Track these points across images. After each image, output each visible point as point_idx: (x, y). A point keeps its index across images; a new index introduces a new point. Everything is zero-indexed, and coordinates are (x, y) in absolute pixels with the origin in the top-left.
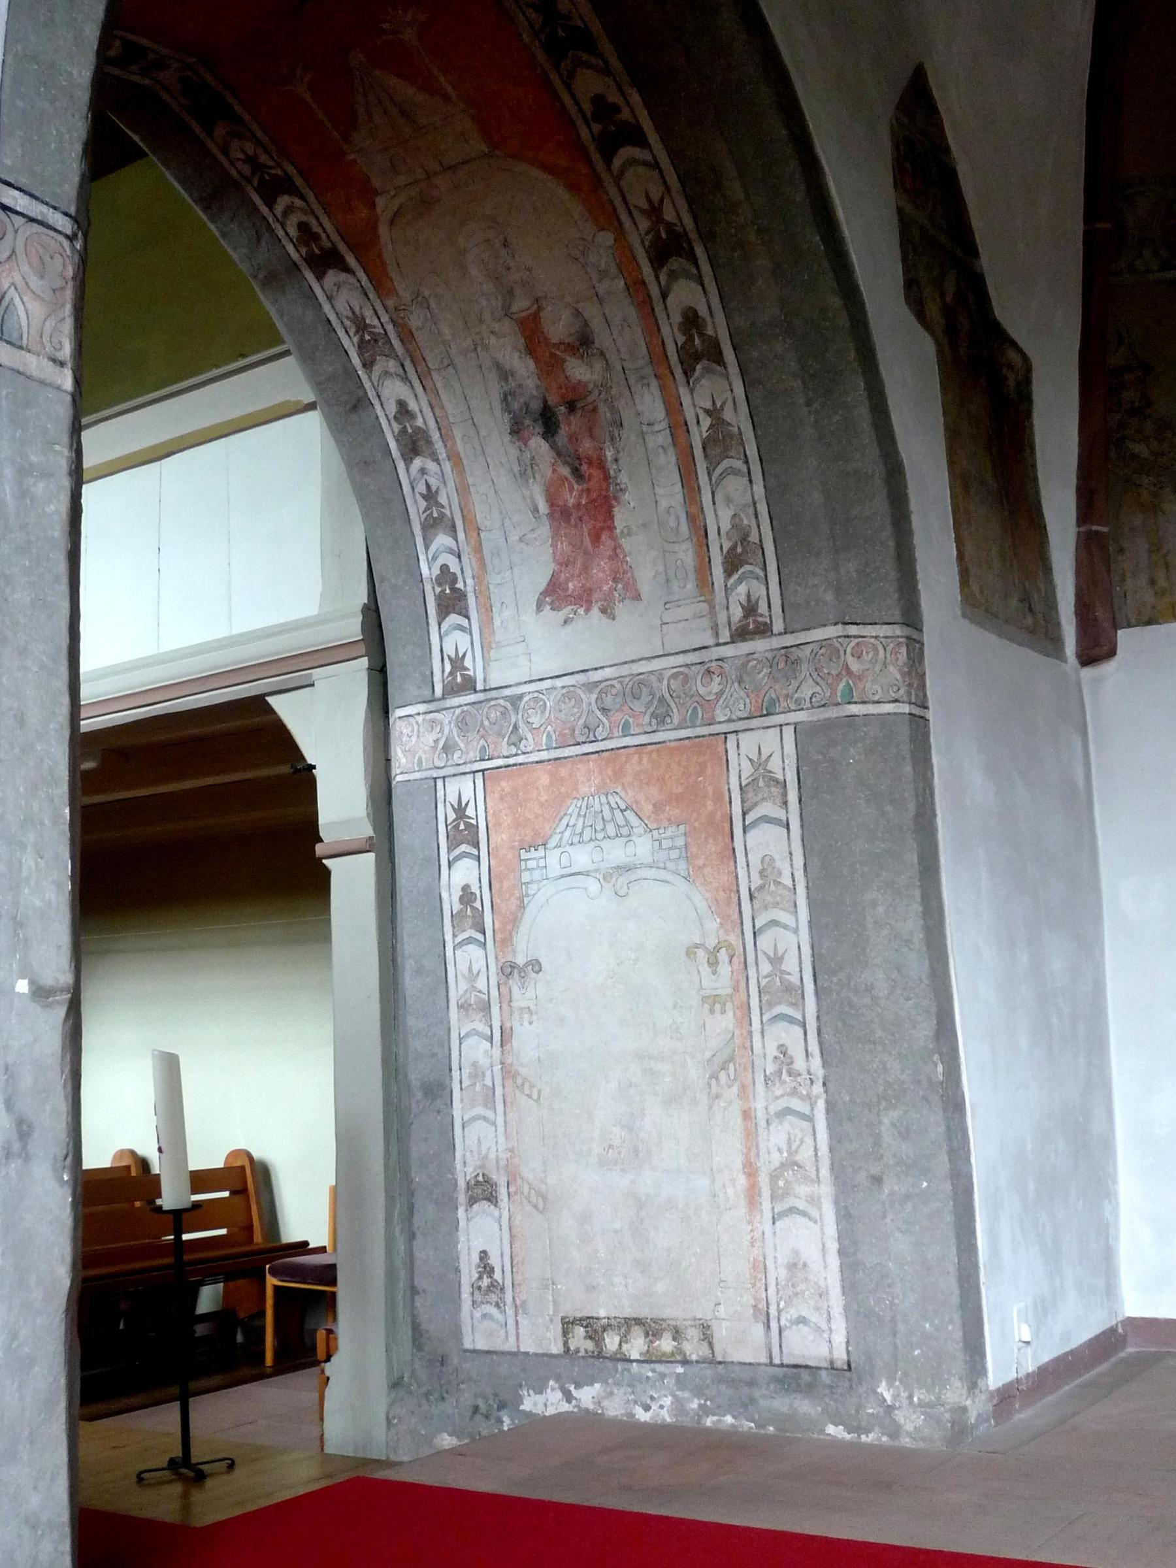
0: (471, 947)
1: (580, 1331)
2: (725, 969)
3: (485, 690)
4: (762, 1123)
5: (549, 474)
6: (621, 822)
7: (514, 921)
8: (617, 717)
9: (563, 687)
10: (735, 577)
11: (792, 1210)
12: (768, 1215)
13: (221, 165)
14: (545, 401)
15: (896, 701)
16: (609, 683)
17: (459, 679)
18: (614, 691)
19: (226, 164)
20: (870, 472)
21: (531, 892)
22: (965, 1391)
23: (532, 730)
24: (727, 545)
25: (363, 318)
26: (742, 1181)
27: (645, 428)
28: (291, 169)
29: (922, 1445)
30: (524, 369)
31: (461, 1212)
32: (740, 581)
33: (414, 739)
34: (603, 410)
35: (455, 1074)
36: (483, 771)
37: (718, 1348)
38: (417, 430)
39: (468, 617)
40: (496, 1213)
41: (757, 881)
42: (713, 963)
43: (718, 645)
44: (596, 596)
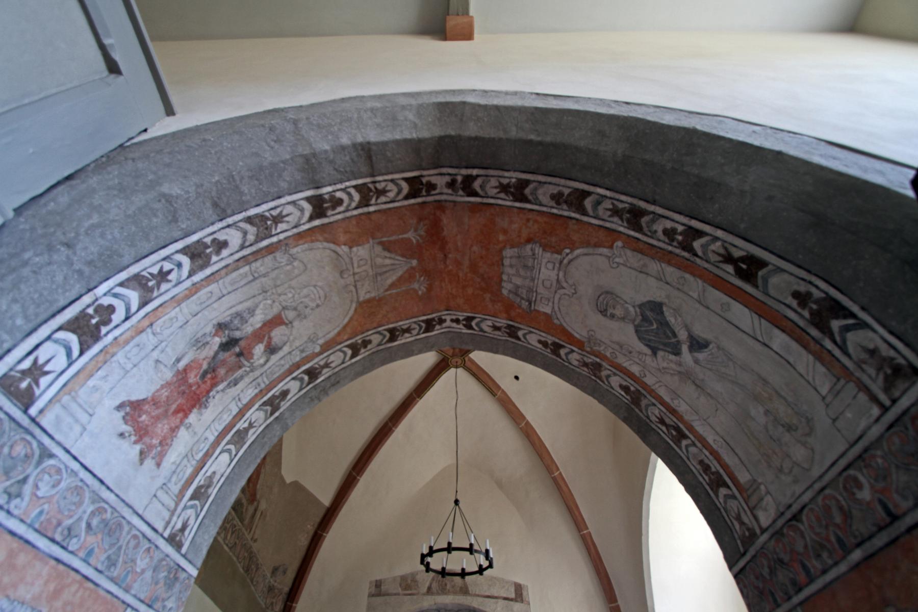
3: (33, 420)
9: (82, 480)
13: (386, 174)
14: (241, 339)
16: (106, 506)
17: (24, 385)
18: (104, 517)
19: (386, 177)
24: (202, 483)
25: (282, 222)
30: (257, 321)
38: (209, 257)
39: (82, 353)
43: (162, 535)
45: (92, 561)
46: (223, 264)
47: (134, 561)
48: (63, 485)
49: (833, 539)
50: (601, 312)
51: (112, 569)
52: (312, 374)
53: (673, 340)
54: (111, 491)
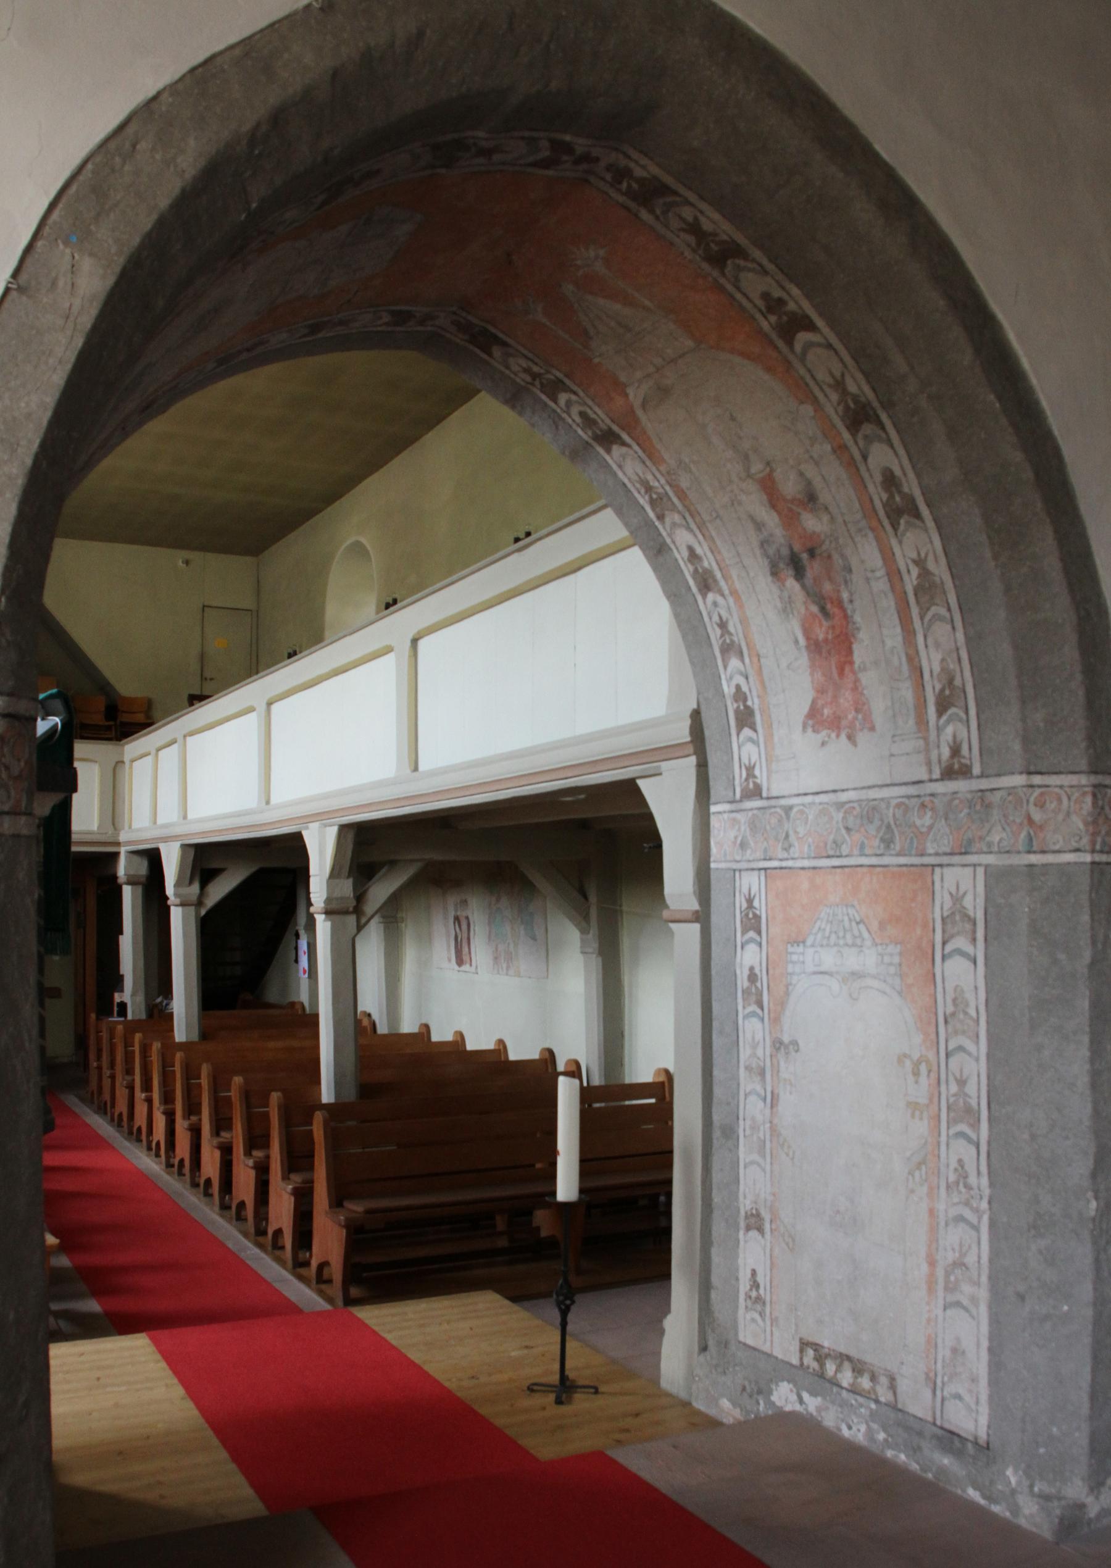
0: (754, 1020)
1: (810, 1353)
2: (923, 1080)
3: (768, 798)
4: (942, 1224)
5: (803, 610)
6: (856, 933)
7: (782, 1004)
8: (857, 837)
9: (820, 804)
10: (944, 718)
11: (958, 1304)
12: (941, 1302)
14: (791, 549)
15: (1077, 850)
16: (851, 805)
18: (855, 813)
20: (1060, 621)
21: (794, 982)
22: (1085, 1490)
23: (798, 838)
24: (938, 687)
25: (648, 482)
26: (925, 1268)
27: (869, 575)
28: (558, 374)
29: (1034, 1530)
30: (771, 520)
31: (741, 1233)
32: (948, 722)
33: (722, 833)
34: (835, 556)
35: (741, 1122)
36: (765, 869)
37: (900, 1399)
39: (755, 731)
40: (763, 1242)
41: (950, 1009)
42: (916, 1073)
43: (931, 780)
44: (844, 723)
46: (709, 554)
48: (811, 817)
51: (892, 846)
54: (847, 790)
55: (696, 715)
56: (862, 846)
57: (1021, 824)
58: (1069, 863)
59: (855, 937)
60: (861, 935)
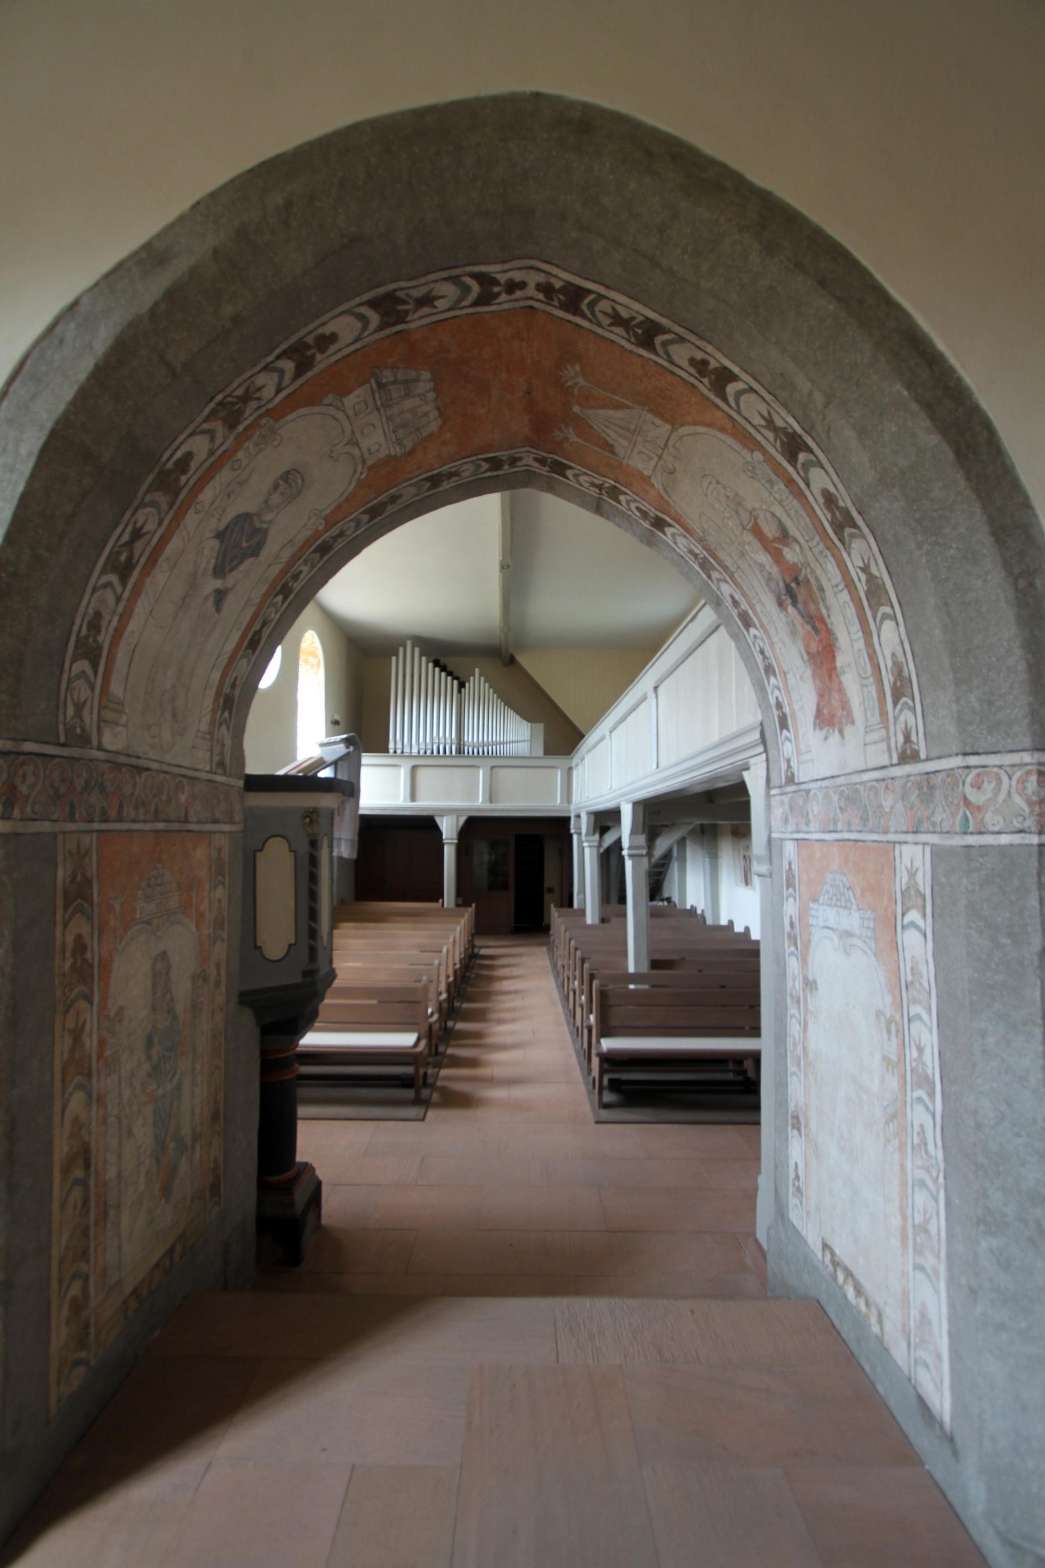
15: (1021, 831)
41: (910, 978)
43: (892, 765)
45: (853, 828)
47: (880, 806)
49: (153, 806)
50: (288, 472)
52: (793, 446)
53: (227, 568)
54: (838, 776)
55: (761, 724)
56: (849, 824)
57: (958, 804)
58: (1011, 845)
59: (846, 901)
60: (850, 900)
